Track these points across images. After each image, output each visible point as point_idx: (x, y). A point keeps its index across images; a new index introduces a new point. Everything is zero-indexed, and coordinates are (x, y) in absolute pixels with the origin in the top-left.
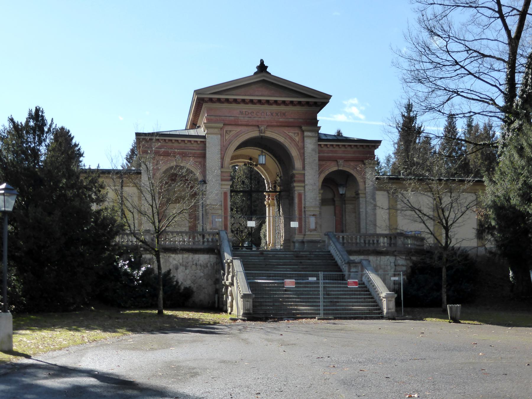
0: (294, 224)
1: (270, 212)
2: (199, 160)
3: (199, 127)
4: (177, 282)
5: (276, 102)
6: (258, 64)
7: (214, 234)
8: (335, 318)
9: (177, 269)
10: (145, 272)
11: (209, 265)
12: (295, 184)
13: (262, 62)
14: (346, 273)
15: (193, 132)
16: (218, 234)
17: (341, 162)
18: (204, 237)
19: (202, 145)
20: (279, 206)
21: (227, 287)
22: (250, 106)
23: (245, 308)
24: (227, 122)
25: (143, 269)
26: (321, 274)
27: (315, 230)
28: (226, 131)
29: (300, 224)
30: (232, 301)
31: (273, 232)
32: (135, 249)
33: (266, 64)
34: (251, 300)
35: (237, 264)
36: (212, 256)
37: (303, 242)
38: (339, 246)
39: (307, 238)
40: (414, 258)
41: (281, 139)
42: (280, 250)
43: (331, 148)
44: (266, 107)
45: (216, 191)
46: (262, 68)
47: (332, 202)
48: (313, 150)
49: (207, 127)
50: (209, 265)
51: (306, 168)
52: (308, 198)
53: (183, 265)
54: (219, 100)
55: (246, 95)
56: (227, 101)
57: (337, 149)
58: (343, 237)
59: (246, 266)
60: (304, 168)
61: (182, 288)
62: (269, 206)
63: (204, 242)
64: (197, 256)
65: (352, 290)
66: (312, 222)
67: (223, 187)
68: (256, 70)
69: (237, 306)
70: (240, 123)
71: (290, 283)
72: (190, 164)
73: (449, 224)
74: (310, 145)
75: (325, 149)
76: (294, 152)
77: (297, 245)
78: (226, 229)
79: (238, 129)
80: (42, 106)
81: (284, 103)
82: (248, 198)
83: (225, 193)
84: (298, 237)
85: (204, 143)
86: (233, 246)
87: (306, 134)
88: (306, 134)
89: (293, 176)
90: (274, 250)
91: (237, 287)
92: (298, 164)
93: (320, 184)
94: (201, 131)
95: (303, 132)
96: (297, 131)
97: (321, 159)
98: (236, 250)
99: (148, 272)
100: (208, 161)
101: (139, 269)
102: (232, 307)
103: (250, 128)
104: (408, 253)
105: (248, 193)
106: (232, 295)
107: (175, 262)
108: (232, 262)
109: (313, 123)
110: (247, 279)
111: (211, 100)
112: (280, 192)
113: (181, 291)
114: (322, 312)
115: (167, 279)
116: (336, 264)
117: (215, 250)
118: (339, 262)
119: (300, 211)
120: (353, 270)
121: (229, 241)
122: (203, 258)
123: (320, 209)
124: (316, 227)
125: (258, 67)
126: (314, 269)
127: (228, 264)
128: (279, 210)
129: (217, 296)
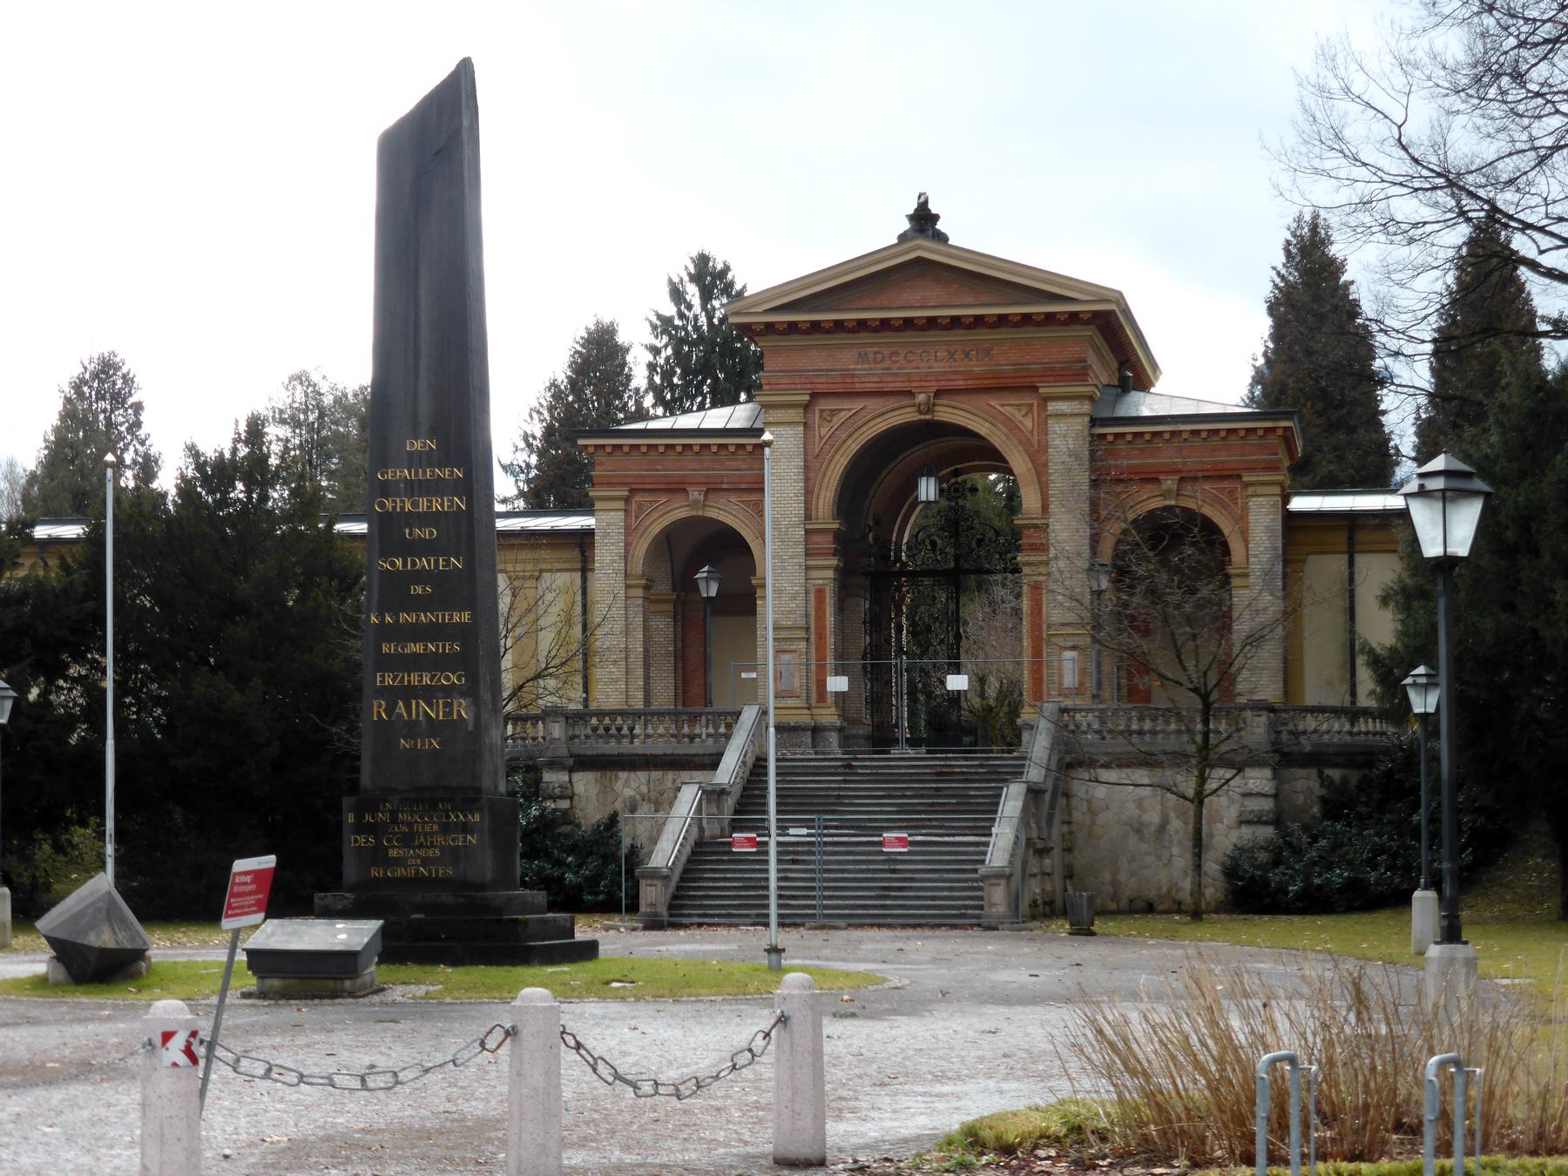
6: (911, 207)
24: (821, 388)
29: (822, 685)
33: (934, 208)
40: (1335, 774)
46: (923, 219)
51: (1053, 508)
53: (649, 801)
55: (891, 309)
60: (1045, 508)
67: (814, 574)
70: (858, 387)
72: (727, 512)
79: (856, 405)
80: (131, 362)
83: (820, 592)
87: (1053, 407)
103: (892, 402)
124: (1081, 684)
125: (911, 218)
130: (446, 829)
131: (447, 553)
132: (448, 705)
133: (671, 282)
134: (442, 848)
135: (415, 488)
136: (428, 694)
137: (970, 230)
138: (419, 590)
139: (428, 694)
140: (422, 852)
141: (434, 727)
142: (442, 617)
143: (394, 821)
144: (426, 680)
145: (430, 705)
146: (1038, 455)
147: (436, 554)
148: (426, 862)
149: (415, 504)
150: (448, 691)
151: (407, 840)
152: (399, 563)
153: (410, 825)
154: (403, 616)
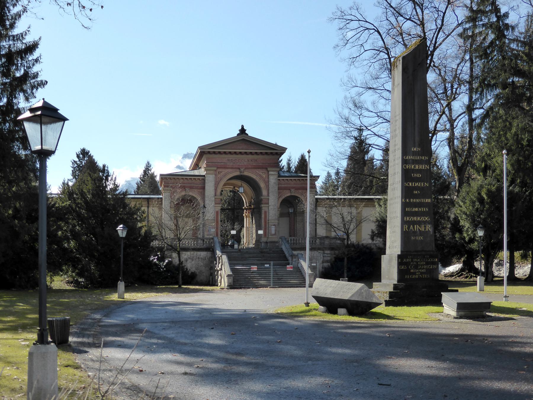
0: (261, 232)
1: (247, 222)
2: (201, 190)
3: (200, 168)
4: (187, 269)
5: (251, 153)
6: (240, 128)
7: (210, 239)
8: (279, 287)
9: (187, 261)
10: (167, 263)
11: (207, 258)
12: (262, 205)
13: (243, 126)
14: (290, 262)
15: (196, 172)
16: (213, 239)
17: (293, 190)
18: (203, 241)
19: (203, 181)
20: (252, 218)
21: (218, 271)
22: (234, 156)
23: (228, 282)
25: (167, 261)
26: (272, 263)
27: (275, 234)
28: (219, 172)
30: (221, 279)
31: (249, 235)
32: (161, 249)
34: (232, 278)
35: (225, 258)
36: (209, 253)
37: (267, 243)
38: (287, 245)
39: (269, 240)
41: (254, 177)
42: (251, 248)
43: (286, 182)
44: (245, 156)
45: (211, 210)
46: (243, 131)
47: (288, 215)
48: (274, 183)
49: (206, 170)
50: (207, 258)
51: (270, 195)
52: (271, 214)
54: (214, 153)
56: (220, 153)
57: (290, 182)
58: (291, 240)
59: (230, 259)
60: (268, 195)
61: (190, 272)
62: (246, 217)
63: (204, 244)
64: (199, 253)
65: (290, 271)
66: (273, 230)
68: (239, 132)
69: (223, 281)
71: (255, 268)
72: (194, 194)
73: (349, 232)
74: (273, 179)
75: (282, 182)
76: (262, 185)
77: (263, 244)
78: (217, 235)
79: (227, 170)
80: (87, 149)
81: (256, 153)
82: (232, 212)
83: (217, 212)
84: (264, 239)
85: (204, 180)
86: (222, 246)
88: (270, 173)
89: (261, 200)
90: (248, 249)
91: (224, 270)
92: (264, 193)
93: (279, 205)
94: (202, 172)
95: (268, 171)
96: (264, 171)
97: (279, 189)
98: (224, 247)
99: (170, 263)
100: (206, 192)
101: (164, 262)
102: (221, 283)
104: (332, 249)
105: (233, 210)
106: (221, 276)
107: (186, 257)
108: (221, 256)
109: (276, 164)
110: (230, 267)
111: (209, 153)
112: (253, 209)
113: (189, 274)
114: (272, 284)
115: (180, 268)
116: (285, 256)
117: (211, 249)
118: (287, 255)
119: (265, 222)
120: (294, 260)
121: (219, 242)
122: (203, 254)
123: (279, 220)
125: (240, 130)
126: (268, 260)
127: (219, 258)
128: (253, 221)
129: (211, 277)
130: (427, 263)
131: (424, 182)
132: (425, 227)
133: (77, 154)
134: (426, 269)
135: (415, 162)
136: (419, 223)
137: (251, 132)
138: (416, 192)
139: (419, 223)
140: (421, 271)
141: (421, 233)
142: (423, 200)
143: (412, 261)
144: (419, 219)
145: (420, 227)
146: (267, 183)
147: (421, 182)
148: (422, 273)
149: (415, 167)
150: (425, 223)
151: (416, 267)
152: (411, 184)
153: (417, 262)
154: (411, 200)
